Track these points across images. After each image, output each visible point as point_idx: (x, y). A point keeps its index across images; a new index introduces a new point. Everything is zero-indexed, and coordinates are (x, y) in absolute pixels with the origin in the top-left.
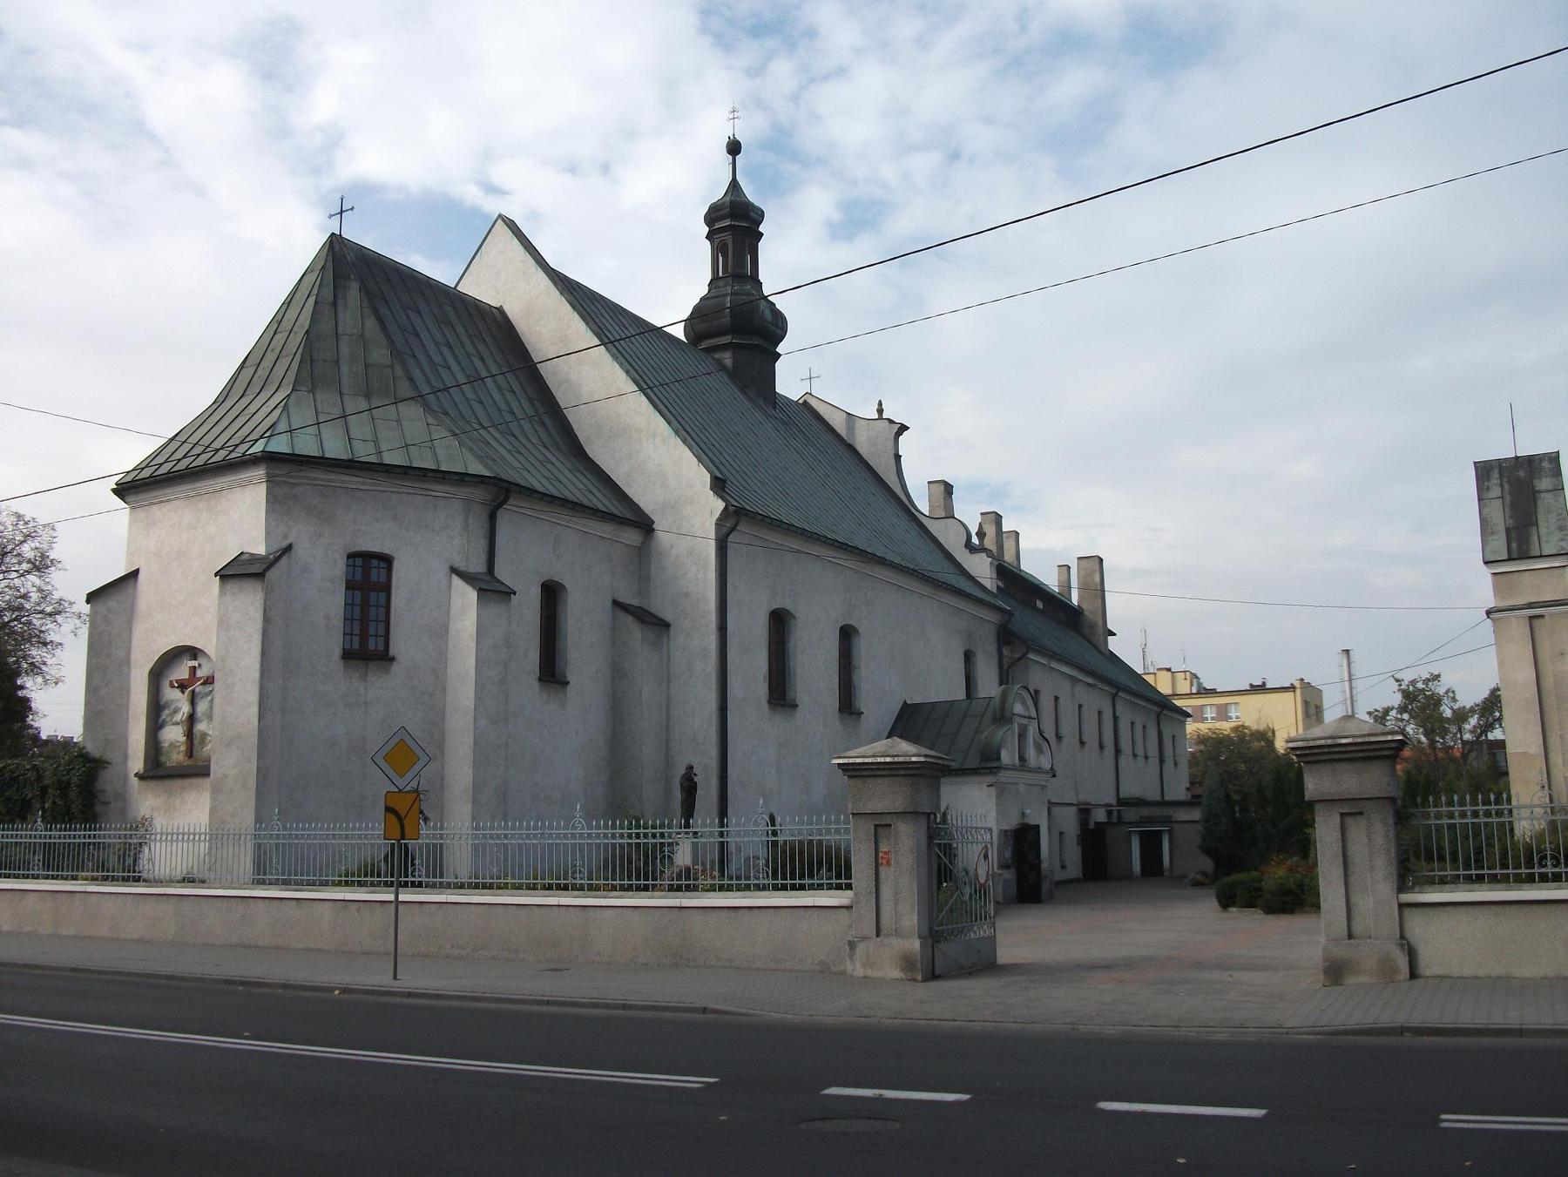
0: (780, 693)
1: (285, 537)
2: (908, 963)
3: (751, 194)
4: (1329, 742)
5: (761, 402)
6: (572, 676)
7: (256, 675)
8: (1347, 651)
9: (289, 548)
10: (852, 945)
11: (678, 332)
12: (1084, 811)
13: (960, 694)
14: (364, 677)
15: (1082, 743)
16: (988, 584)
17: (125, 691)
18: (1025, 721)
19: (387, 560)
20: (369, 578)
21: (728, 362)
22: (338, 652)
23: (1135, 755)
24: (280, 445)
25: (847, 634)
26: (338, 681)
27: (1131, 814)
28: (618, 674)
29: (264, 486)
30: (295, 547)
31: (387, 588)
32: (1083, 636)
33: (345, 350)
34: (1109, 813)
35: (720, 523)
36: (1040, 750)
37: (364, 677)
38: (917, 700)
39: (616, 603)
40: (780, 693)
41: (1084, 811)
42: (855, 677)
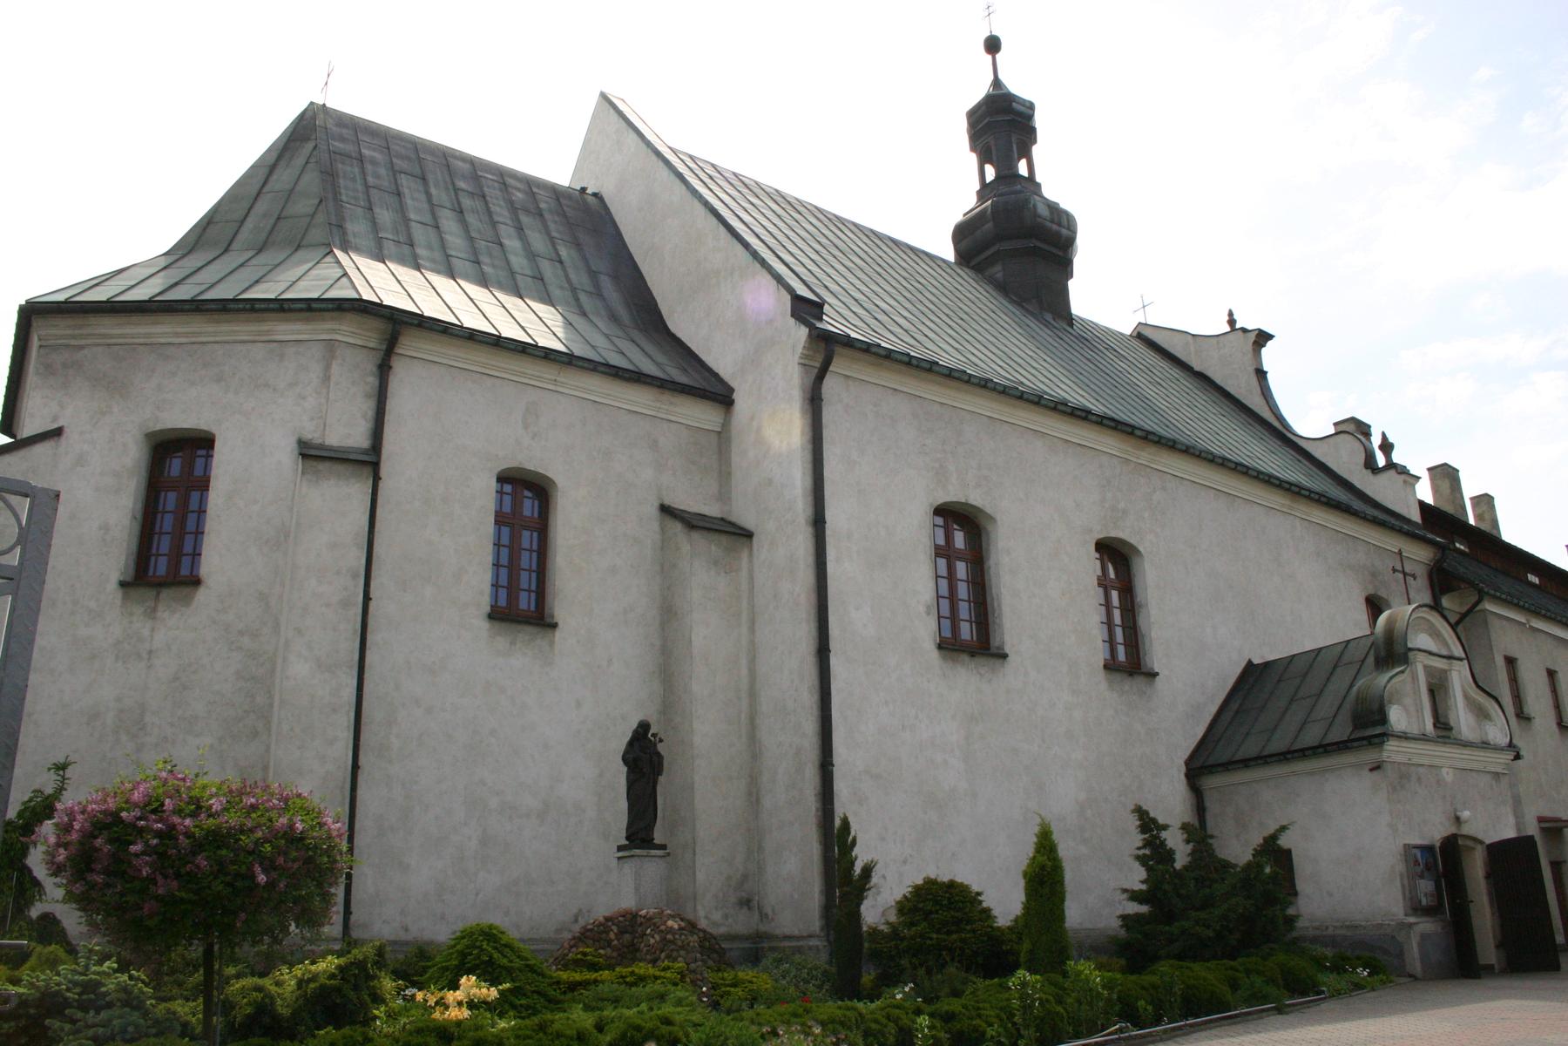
0: (972, 632)
1: (55, 419)
3: (1017, 86)
5: (1049, 317)
11: (948, 253)
14: (151, 613)
18: (1440, 664)
21: (999, 275)
36: (1482, 714)
37: (151, 613)
39: (666, 510)
40: (972, 632)
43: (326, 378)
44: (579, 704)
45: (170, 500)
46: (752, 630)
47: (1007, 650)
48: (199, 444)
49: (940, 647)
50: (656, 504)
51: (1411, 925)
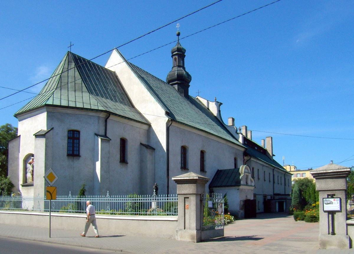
1: (52, 126)
2: (192, 237)
4: (325, 172)
6: (129, 161)
7: (44, 160)
8: (332, 161)
9: (53, 129)
10: (177, 231)
12: (265, 196)
13: (233, 167)
15: (265, 180)
16: (241, 142)
17: (18, 165)
18: (248, 174)
19: (79, 132)
20: (74, 137)
22: (66, 154)
23: (278, 184)
24: (50, 102)
25: (202, 153)
26: (66, 162)
27: (277, 197)
28: (142, 161)
29: (46, 113)
30: (54, 128)
31: (79, 139)
32: (267, 156)
33: (70, 80)
34: (271, 197)
35: (167, 124)
36: (252, 182)
38: (221, 169)
41: (265, 196)
42: (205, 163)
44: (131, 176)
47: (189, 169)
50: (140, 143)
51: (240, 211)
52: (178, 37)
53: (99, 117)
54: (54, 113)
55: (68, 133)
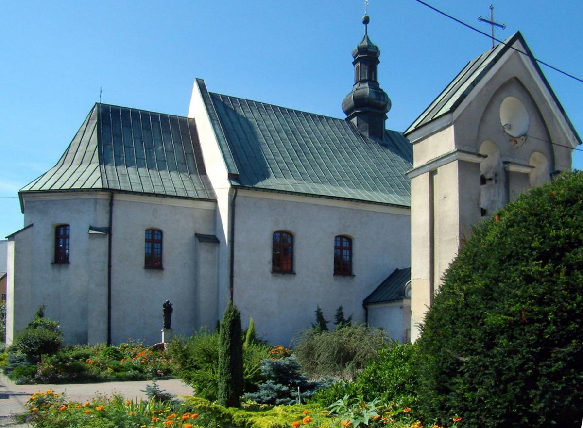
3: (374, 42)
9: (32, 225)
20: (61, 233)
30: (34, 224)
31: (161, 242)
43: (95, 210)
45: (61, 241)
46: (218, 268)
48: (66, 226)
49: (272, 273)
50: (194, 233)
52: (366, 26)
53: (96, 200)
54: (34, 202)
55: (146, 233)
